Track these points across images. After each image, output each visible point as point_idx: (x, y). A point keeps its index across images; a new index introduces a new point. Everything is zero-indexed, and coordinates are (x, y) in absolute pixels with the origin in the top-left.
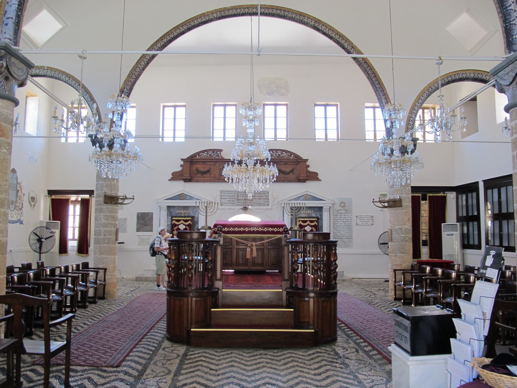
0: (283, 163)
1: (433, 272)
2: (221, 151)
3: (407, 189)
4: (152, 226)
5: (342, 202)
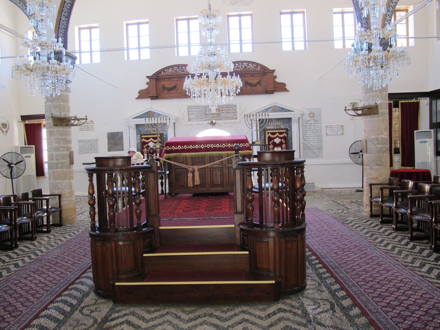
0: (250, 75)
1: (418, 189)
2: (186, 66)
3: (384, 94)
4: (122, 145)
5: (311, 113)
